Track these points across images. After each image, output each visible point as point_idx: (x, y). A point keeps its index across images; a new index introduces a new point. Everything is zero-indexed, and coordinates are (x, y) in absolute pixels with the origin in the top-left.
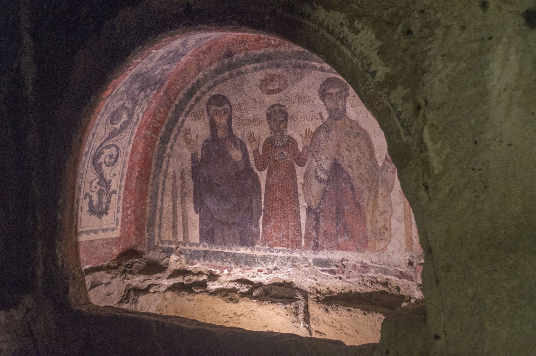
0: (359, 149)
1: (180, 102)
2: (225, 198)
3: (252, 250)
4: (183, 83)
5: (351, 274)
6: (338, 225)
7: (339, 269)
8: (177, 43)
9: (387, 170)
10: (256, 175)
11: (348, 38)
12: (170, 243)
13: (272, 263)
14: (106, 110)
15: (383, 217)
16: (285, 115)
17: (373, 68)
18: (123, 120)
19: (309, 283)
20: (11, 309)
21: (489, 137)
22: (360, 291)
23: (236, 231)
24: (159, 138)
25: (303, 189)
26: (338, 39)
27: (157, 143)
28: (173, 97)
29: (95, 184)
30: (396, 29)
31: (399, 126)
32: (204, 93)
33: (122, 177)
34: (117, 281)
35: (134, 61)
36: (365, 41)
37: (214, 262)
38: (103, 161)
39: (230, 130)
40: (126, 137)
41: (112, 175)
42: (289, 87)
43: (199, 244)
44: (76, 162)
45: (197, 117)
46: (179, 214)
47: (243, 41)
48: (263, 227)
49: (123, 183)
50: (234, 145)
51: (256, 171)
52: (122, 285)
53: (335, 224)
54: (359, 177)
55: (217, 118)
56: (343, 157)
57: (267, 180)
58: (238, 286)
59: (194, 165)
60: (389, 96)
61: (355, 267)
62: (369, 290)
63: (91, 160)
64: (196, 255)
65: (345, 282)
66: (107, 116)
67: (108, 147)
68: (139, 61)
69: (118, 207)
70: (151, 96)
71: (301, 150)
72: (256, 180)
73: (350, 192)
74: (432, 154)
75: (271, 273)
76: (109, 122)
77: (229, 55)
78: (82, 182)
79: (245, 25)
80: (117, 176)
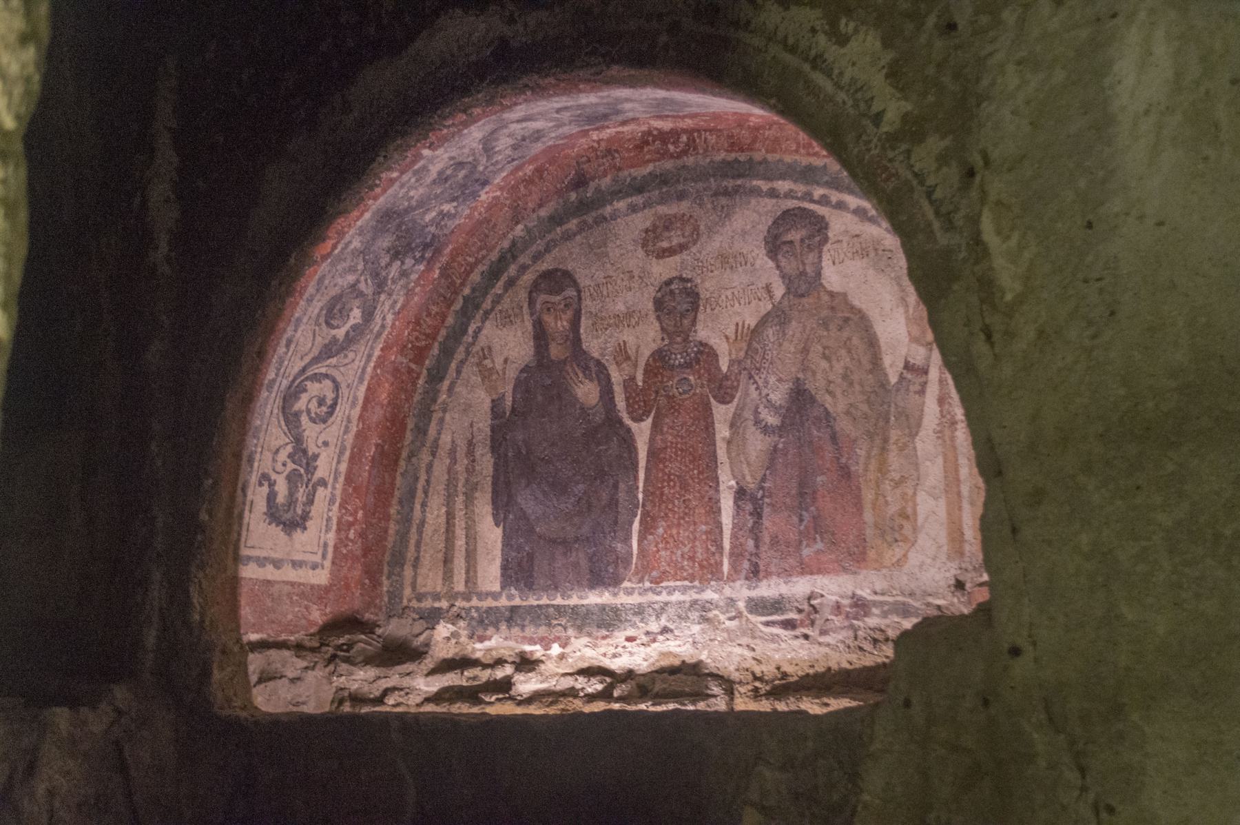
0: (849, 352)
1: (473, 290)
2: (560, 488)
3: (615, 595)
4: (481, 249)
5: (829, 626)
6: (801, 520)
7: (804, 618)
8: (475, 135)
9: (908, 390)
10: (629, 430)
11: (826, 56)
12: (437, 597)
13: (658, 617)
14: (318, 290)
15: (898, 491)
16: (694, 297)
17: (876, 107)
18: (352, 322)
19: (738, 659)
20: (82, 709)
21: (1116, 209)
22: (848, 666)
23: (580, 557)
24: (425, 371)
25: (728, 451)
26: (806, 60)
27: (421, 382)
28: (459, 281)
29: (283, 456)
30: (923, 24)
31: (930, 215)
32: (524, 268)
33: (341, 453)
34: (316, 677)
35: (383, 175)
36: (860, 57)
37: (530, 631)
38: (304, 408)
39: (577, 340)
40: (357, 362)
41: (320, 443)
42: (704, 239)
43: (500, 594)
44: (248, 400)
45: (507, 320)
46: (460, 533)
47: (609, 152)
48: (641, 540)
49: (343, 467)
50: (584, 372)
51: (628, 421)
52: (327, 688)
53: (795, 519)
54: (848, 413)
55: (548, 319)
56: (814, 373)
57: (652, 440)
58: (581, 682)
59: (497, 422)
60: (909, 158)
61: (839, 607)
62: (868, 661)
63: (279, 402)
64: (493, 618)
65: (817, 646)
66: (320, 304)
67: (317, 378)
68: (395, 175)
69: (329, 519)
70: (414, 277)
71: (724, 368)
72: (628, 442)
73: (829, 449)
74: (999, 262)
75: (654, 641)
76: (322, 320)
77: (580, 182)
78: (256, 445)
79: (618, 62)
80: (332, 445)
